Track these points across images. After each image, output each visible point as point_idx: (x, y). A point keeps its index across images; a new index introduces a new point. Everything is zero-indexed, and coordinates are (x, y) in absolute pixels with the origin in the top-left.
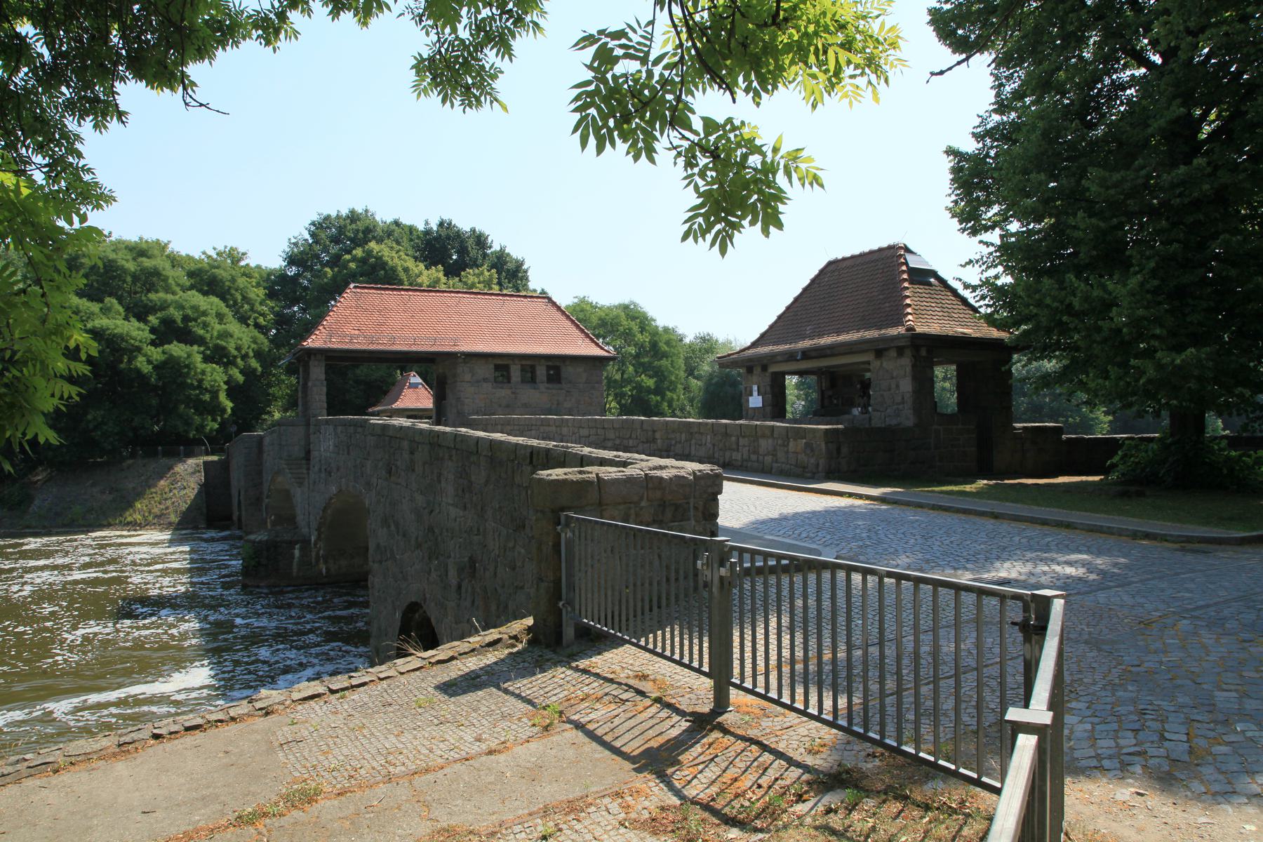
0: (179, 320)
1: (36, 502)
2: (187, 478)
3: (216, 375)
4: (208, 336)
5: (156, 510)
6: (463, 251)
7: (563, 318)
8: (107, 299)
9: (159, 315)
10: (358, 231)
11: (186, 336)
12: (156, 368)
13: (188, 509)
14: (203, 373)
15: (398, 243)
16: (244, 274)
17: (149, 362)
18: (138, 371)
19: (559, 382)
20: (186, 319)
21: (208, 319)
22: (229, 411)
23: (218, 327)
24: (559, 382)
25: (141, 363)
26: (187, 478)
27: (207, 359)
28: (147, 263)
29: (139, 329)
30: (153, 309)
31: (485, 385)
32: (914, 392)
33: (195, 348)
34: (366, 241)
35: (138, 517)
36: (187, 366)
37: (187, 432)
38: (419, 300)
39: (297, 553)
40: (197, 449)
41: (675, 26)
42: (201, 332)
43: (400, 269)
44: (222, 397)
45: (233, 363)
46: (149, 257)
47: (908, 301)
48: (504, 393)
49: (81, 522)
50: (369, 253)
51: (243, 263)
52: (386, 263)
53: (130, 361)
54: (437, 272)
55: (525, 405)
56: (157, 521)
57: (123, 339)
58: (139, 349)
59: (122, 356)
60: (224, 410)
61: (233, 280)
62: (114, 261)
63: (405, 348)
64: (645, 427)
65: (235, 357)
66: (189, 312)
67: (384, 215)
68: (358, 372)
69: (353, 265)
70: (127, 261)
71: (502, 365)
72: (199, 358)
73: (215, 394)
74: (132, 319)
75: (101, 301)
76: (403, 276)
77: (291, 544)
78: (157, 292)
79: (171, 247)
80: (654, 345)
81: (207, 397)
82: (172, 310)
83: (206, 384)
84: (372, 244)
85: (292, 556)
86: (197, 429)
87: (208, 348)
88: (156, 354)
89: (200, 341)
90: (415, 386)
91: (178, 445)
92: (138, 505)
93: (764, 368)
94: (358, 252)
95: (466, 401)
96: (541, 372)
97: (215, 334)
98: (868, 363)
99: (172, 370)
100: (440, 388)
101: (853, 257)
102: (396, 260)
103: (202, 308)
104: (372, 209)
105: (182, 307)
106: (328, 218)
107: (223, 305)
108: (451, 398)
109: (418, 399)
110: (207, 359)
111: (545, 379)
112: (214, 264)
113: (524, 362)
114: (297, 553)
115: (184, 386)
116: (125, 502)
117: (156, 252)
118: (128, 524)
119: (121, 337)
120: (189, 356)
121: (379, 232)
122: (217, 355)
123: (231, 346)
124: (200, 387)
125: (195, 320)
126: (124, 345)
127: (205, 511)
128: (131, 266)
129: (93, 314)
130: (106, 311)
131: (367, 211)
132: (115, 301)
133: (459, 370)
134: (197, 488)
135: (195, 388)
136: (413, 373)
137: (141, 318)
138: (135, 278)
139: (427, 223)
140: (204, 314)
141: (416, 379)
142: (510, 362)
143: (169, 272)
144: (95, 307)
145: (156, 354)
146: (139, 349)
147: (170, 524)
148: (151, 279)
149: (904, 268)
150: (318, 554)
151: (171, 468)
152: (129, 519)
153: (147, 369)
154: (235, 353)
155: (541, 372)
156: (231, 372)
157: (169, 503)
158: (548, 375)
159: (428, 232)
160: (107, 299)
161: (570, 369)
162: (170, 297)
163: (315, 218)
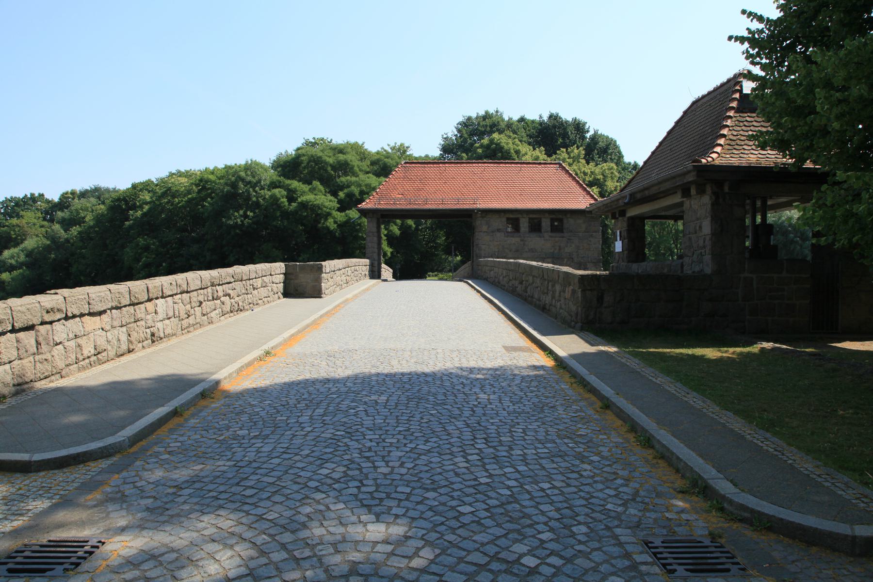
6: (565, 135)
7: (570, 179)
8: (314, 182)
9: (346, 191)
10: (486, 126)
12: (339, 226)
15: (515, 132)
17: (335, 222)
18: (328, 228)
19: (563, 232)
22: (389, 254)
24: (563, 232)
25: (330, 224)
28: (341, 157)
29: (330, 201)
31: (498, 234)
32: (713, 234)
34: (491, 132)
38: (528, 171)
46: (344, 154)
47: (725, 131)
48: (515, 240)
50: (492, 141)
52: (502, 148)
54: (540, 153)
55: (532, 250)
57: (319, 208)
58: (329, 214)
62: (321, 157)
63: (434, 207)
66: (364, 188)
67: (511, 113)
70: (330, 157)
71: (513, 218)
74: (328, 195)
75: (310, 183)
76: (515, 156)
79: (334, 142)
82: (353, 188)
84: (496, 136)
88: (340, 217)
93: (623, 213)
95: (483, 247)
96: (546, 223)
98: (681, 204)
101: (709, 93)
102: (511, 146)
105: (359, 185)
106: (469, 118)
111: (549, 229)
113: (531, 216)
115: (357, 238)
117: (349, 150)
119: (319, 207)
121: (503, 125)
128: (331, 160)
130: (312, 190)
131: (497, 112)
132: (318, 183)
137: (334, 194)
138: (334, 168)
139: (541, 117)
142: (519, 216)
144: (306, 188)
146: (329, 214)
148: (344, 168)
149: (737, 96)
155: (546, 223)
156: (391, 228)
158: (552, 225)
159: (541, 123)
160: (314, 182)
161: (571, 221)
163: (461, 119)
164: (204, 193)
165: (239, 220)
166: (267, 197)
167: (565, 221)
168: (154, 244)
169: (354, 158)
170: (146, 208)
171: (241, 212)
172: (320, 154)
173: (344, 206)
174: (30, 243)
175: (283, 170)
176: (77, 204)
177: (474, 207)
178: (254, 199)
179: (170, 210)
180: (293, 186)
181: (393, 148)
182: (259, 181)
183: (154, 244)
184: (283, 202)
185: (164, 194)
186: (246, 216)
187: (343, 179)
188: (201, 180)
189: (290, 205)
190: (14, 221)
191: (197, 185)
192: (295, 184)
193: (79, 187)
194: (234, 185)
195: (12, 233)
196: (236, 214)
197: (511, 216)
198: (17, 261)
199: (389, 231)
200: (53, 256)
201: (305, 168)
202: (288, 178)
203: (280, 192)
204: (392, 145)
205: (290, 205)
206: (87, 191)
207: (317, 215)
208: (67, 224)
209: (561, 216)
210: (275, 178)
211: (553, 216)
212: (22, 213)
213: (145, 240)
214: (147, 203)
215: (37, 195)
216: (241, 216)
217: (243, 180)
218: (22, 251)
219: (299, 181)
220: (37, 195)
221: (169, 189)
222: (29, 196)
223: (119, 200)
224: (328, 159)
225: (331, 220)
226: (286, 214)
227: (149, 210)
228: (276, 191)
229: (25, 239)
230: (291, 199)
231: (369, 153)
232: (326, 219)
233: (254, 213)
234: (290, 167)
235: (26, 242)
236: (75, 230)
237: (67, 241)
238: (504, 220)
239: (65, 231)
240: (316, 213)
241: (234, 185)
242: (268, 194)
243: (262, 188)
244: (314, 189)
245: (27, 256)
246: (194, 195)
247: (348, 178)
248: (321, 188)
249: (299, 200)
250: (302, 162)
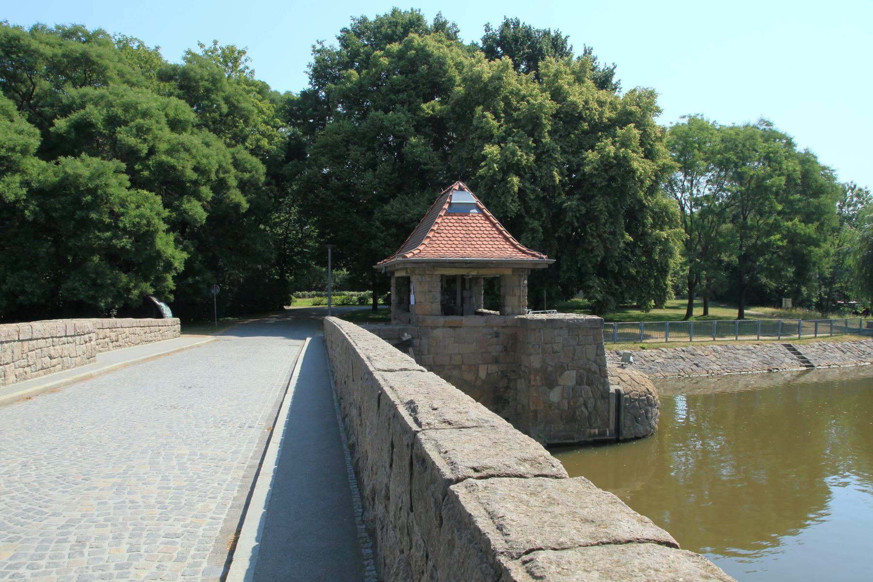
4: (144, 149)
20: (113, 122)
36: (93, 192)
41: (531, 551)
42: (132, 141)
43: (450, 62)
65: (196, 183)
66: (120, 112)
68: (387, 208)
69: (385, 61)
80: (806, 175)
82: (90, 107)
90: (462, 210)
94: (395, 47)
115: (85, 224)
123: (186, 168)
124: (114, 227)
173: (51, 149)
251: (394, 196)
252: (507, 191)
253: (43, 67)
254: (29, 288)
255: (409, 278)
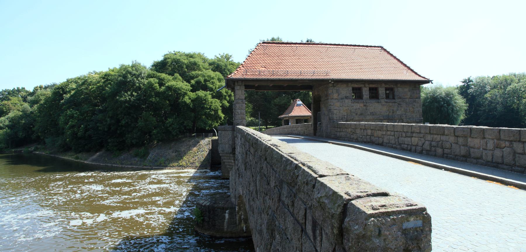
0: (203, 82)
1: (150, 155)
2: (205, 147)
3: (216, 103)
4: (214, 87)
5: (191, 161)
9: (195, 80)
11: (205, 88)
12: (192, 101)
13: (204, 160)
14: (211, 103)
16: (231, 64)
17: (190, 99)
18: (185, 102)
20: (205, 81)
21: (214, 80)
22: (223, 118)
23: (218, 84)
25: (187, 99)
26: (205, 147)
27: (213, 97)
28: (192, 60)
29: (186, 85)
30: (193, 78)
31: (347, 101)
33: (208, 92)
35: (184, 163)
36: (205, 100)
37: (205, 127)
39: (227, 216)
40: (209, 134)
42: (211, 86)
44: (220, 113)
45: (225, 99)
48: (358, 106)
49: (163, 164)
51: (230, 60)
53: (182, 99)
55: (372, 114)
56: (191, 165)
57: (179, 90)
58: (185, 94)
59: (180, 96)
60: (220, 118)
61: (226, 66)
62: (179, 59)
64: (401, 120)
65: (225, 96)
66: (207, 78)
68: (275, 101)
70: (185, 59)
72: (210, 96)
73: (216, 111)
74: (185, 82)
75: (173, 75)
77: (224, 210)
78: (195, 71)
81: (213, 113)
82: (200, 77)
83: (212, 107)
85: (224, 217)
86: (209, 126)
87: (214, 92)
88: (193, 95)
89: (211, 90)
90: (299, 105)
91: (204, 132)
92: (185, 158)
95: (335, 111)
97: (217, 87)
99: (199, 102)
100: (316, 106)
103: (212, 76)
104: (280, 37)
105: (204, 76)
107: (221, 75)
108: (324, 109)
109: (301, 111)
110: (213, 97)
111: (385, 96)
112: (219, 60)
113: (371, 86)
114: (227, 216)
115: (203, 108)
116: (179, 156)
117: (196, 56)
118: (180, 166)
120: (206, 96)
122: (218, 96)
124: (210, 108)
125: (209, 81)
126: (179, 92)
127: (210, 161)
128: (186, 62)
129: (169, 80)
131: (278, 38)
132: (178, 75)
133: (330, 91)
134: (208, 151)
135: (208, 109)
136: (298, 100)
138: (187, 67)
140: (213, 78)
141: (299, 102)
143: (200, 63)
144: (170, 78)
145: (193, 95)
147: (196, 167)
148: (193, 66)
150: (240, 217)
151: (199, 142)
152: (181, 164)
153: (188, 101)
154: (225, 94)
156: (224, 102)
157: (196, 157)
161: (400, 89)
162: (200, 72)
164: (107, 83)
165: (127, 98)
166: (146, 83)
167: (396, 90)
168: (76, 113)
169: (199, 60)
170: (73, 92)
171: (129, 93)
172: (179, 58)
173: (194, 89)
174: (11, 115)
175: (156, 68)
176: (39, 92)
177: (328, 77)
178: (137, 85)
179: (87, 94)
180: (162, 77)
181: (222, 57)
182: (141, 74)
183: (76, 113)
184: (156, 86)
185: (83, 84)
186: (132, 95)
187: (194, 73)
188: (106, 75)
189: (160, 88)
190: (6, 102)
191: (104, 78)
192: (163, 75)
193: (44, 84)
194: (125, 76)
195: (4, 108)
196: (126, 94)
197: (356, 86)
198: (3, 124)
199: (223, 104)
200: (23, 121)
201: (169, 66)
202: (159, 72)
203: (154, 80)
204: (222, 54)
205: (160, 88)
206: (48, 86)
207: (178, 94)
208: (32, 103)
209: (392, 86)
210: (151, 72)
211: (387, 86)
212: (10, 98)
213: (71, 111)
214: (73, 89)
215: (21, 88)
216: (129, 95)
217: (130, 73)
218: (7, 119)
219: (166, 74)
220: (21, 88)
221: (86, 81)
222: (16, 89)
223: (58, 88)
224: (184, 61)
225: (187, 97)
226: (158, 94)
227: (75, 94)
228: (152, 80)
229: (10, 112)
230: (161, 84)
231: (208, 59)
232: (184, 97)
233: (138, 93)
234: (160, 66)
235: (10, 114)
236: (36, 107)
237: (32, 113)
238: (351, 89)
239: (31, 107)
240: (177, 93)
241: (125, 76)
242: (146, 82)
243: (143, 78)
244: (176, 78)
245: (10, 121)
246: (101, 84)
247: (197, 72)
248: (180, 78)
249: (167, 85)
250: (167, 62)
251: (277, 97)
252: (309, 96)
253: (185, 66)
254: (190, 125)
255: (362, 99)
